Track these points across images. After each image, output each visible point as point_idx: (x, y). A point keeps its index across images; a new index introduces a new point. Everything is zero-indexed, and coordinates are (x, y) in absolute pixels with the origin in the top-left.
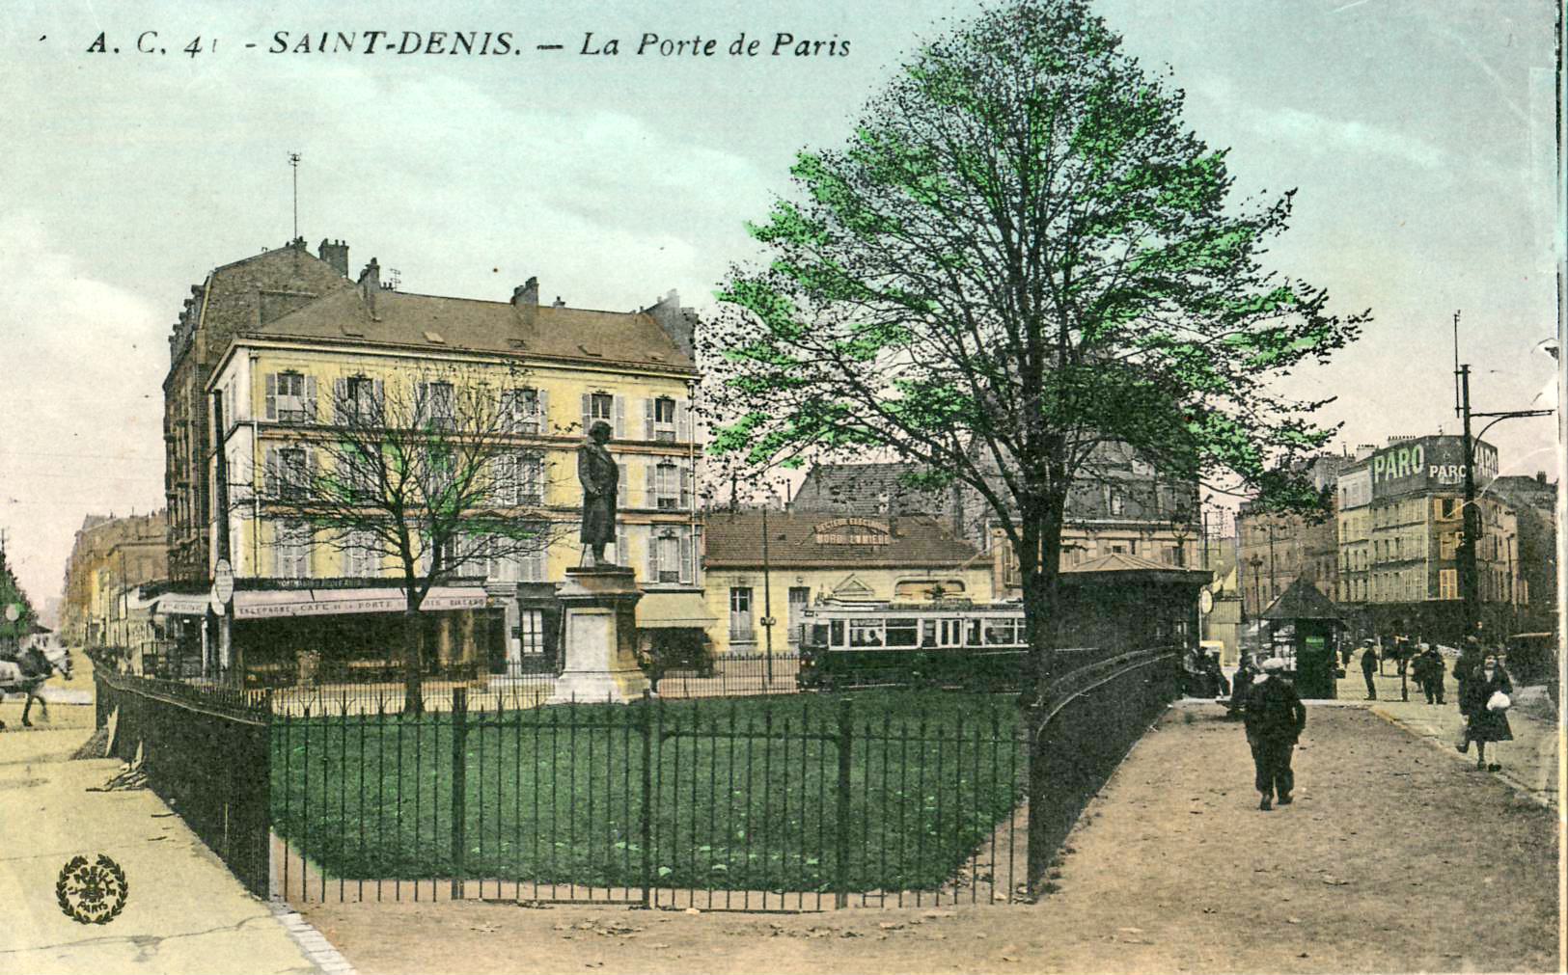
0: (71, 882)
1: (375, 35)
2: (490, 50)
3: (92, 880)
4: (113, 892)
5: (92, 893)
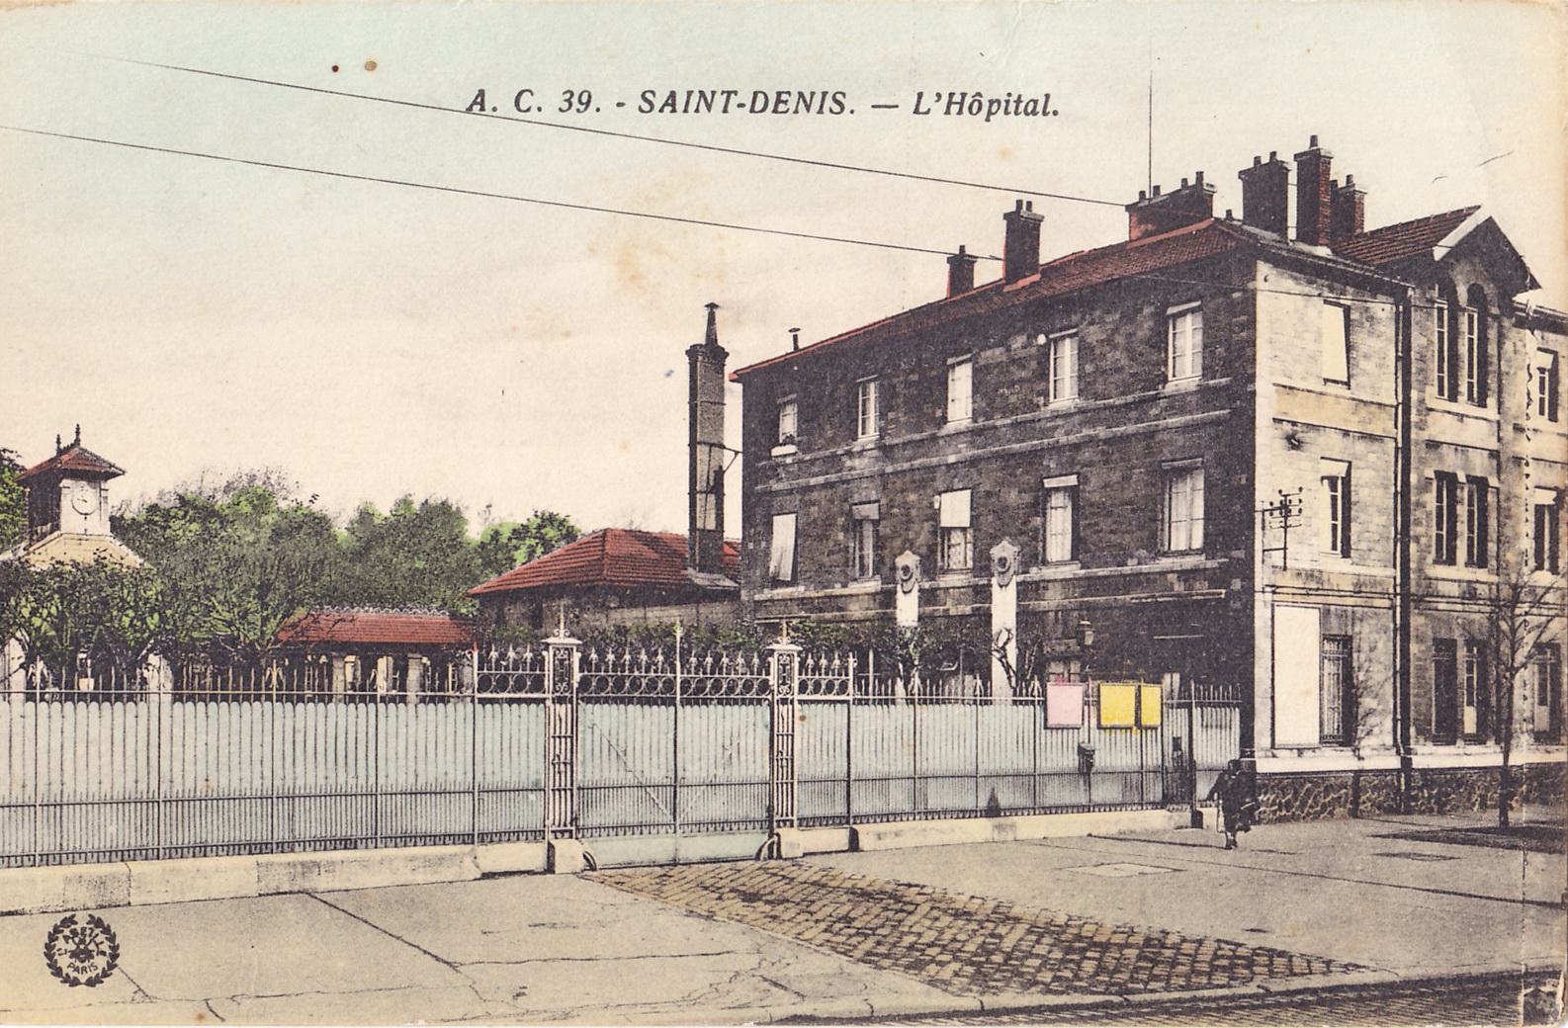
0: (60, 943)
1: (729, 93)
2: (826, 109)
3: (82, 941)
4: (103, 953)
5: (82, 954)
